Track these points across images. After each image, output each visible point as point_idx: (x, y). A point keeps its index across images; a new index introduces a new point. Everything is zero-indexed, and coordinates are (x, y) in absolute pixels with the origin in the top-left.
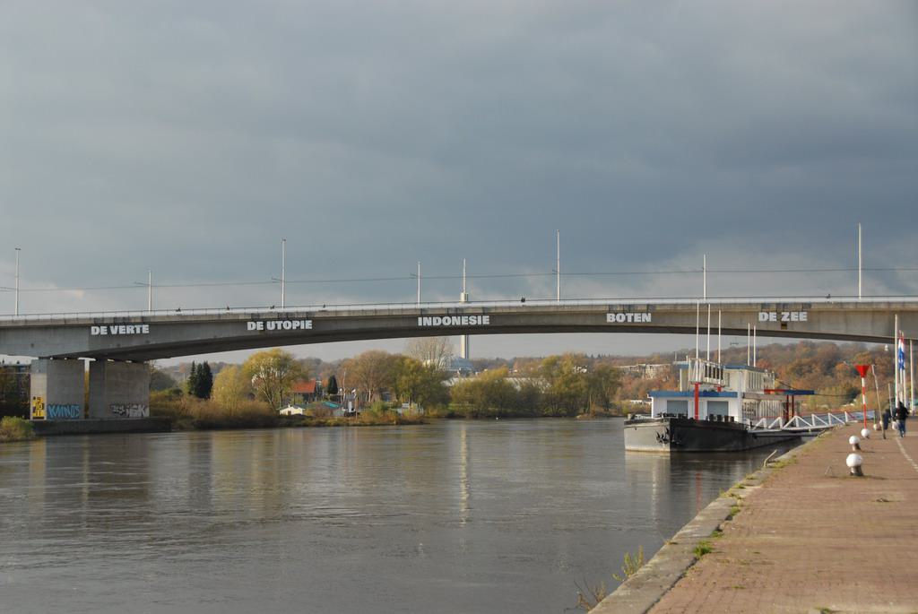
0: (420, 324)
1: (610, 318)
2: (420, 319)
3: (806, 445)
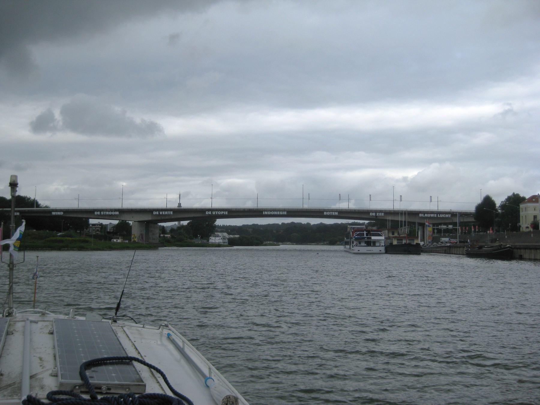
0: (264, 213)
1: (325, 213)
2: (264, 212)
3: (535, 267)
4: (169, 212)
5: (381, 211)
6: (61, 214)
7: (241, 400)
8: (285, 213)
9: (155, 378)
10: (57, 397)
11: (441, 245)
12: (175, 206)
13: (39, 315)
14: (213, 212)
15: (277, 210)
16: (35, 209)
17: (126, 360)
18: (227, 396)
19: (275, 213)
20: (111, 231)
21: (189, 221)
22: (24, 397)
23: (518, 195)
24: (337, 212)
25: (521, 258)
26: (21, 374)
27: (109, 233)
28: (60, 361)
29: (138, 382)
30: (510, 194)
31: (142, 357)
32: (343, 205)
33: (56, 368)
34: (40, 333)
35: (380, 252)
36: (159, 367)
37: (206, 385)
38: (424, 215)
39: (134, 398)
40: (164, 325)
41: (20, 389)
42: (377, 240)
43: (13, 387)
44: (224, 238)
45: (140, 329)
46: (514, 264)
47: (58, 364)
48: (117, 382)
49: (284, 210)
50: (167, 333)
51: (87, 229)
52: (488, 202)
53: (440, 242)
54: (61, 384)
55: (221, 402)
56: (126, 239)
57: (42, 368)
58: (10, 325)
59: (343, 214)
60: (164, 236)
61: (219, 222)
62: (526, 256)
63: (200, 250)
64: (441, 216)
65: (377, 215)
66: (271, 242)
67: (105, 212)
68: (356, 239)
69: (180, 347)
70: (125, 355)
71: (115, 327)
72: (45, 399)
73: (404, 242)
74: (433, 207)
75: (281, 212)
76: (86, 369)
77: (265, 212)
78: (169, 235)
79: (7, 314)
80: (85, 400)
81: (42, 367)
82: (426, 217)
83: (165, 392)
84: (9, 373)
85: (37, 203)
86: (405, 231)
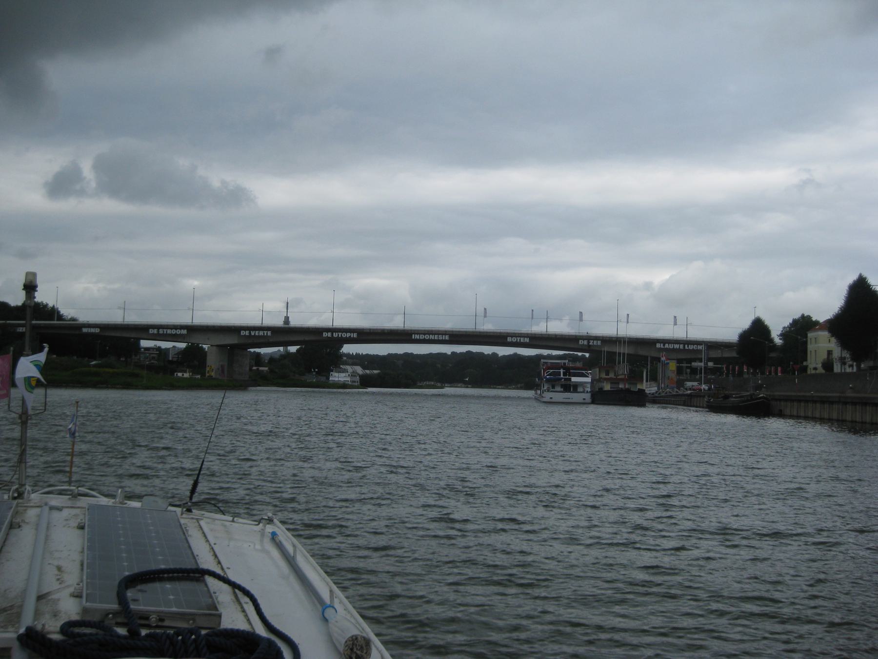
1: (509, 339)
2: (413, 335)
4: (265, 332)
5: (596, 338)
6: (97, 331)
7: (374, 644)
8: (447, 338)
9: (240, 603)
10: (77, 630)
11: (677, 392)
12: (279, 322)
13: (68, 497)
14: (334, 334)
15: (433, 332)
16: (55, 322)
17: (197, 574)
18: (353, 636)
19: (432, 337)
20: (175, 359)
21: (298, 347)
22: (22, 630)
23: (809, 317)
24: (527, 337)
25: (781, 415)
26: (24, 593)
27: (171, 362)
28: (87, 572)
29: (209, 610)
30: (797, 316)
31: (222, 569)
32: (539, 328)
33: (81, 584)
34: (64, 526)
35: (551, 400)
36: (248, 587)
37: (323, 615)
38: (664, 345)
39: (198, 636)
40: (266, 518)
41: (19, 615)
42: (580, 382)
43: (9, 612)
44: (353, 374)
45: (228, 524)
46: (775, 424)
47: (85, 577)
48: (174, 609)
49: (444, 333)
50: (271, 531)
51: (136, 355)
52: (759, 328)
53: (683, 387)
54: (85, 611)
55: (343, 645)
56: (198, 374)
57: (60, 584)
58: (16, 513)
59: (537, 340)
60: (258, 369)
61: (348, 349)
62: (787, 412)
63: (307, 392)
64: (691, 347)
65: (590, 344)
66: (433, 383)
67: (165, 330)
68: (548, 381)
69: (288, 552)
70: (194, 567)
71: (185, 520)
72: (58, 633)
73: (621, 386)
74: (679, 333)
75: (440, 336)
76: (127, 588)
77: (416, 335)
78: (266, 369)
79: (16, 495)
80: (119, 636)
81: (59, 582)
82: (667, 348)
83: (253, 629)
84: (5, 591)
85: (58, 312)
86: (623, 370)
